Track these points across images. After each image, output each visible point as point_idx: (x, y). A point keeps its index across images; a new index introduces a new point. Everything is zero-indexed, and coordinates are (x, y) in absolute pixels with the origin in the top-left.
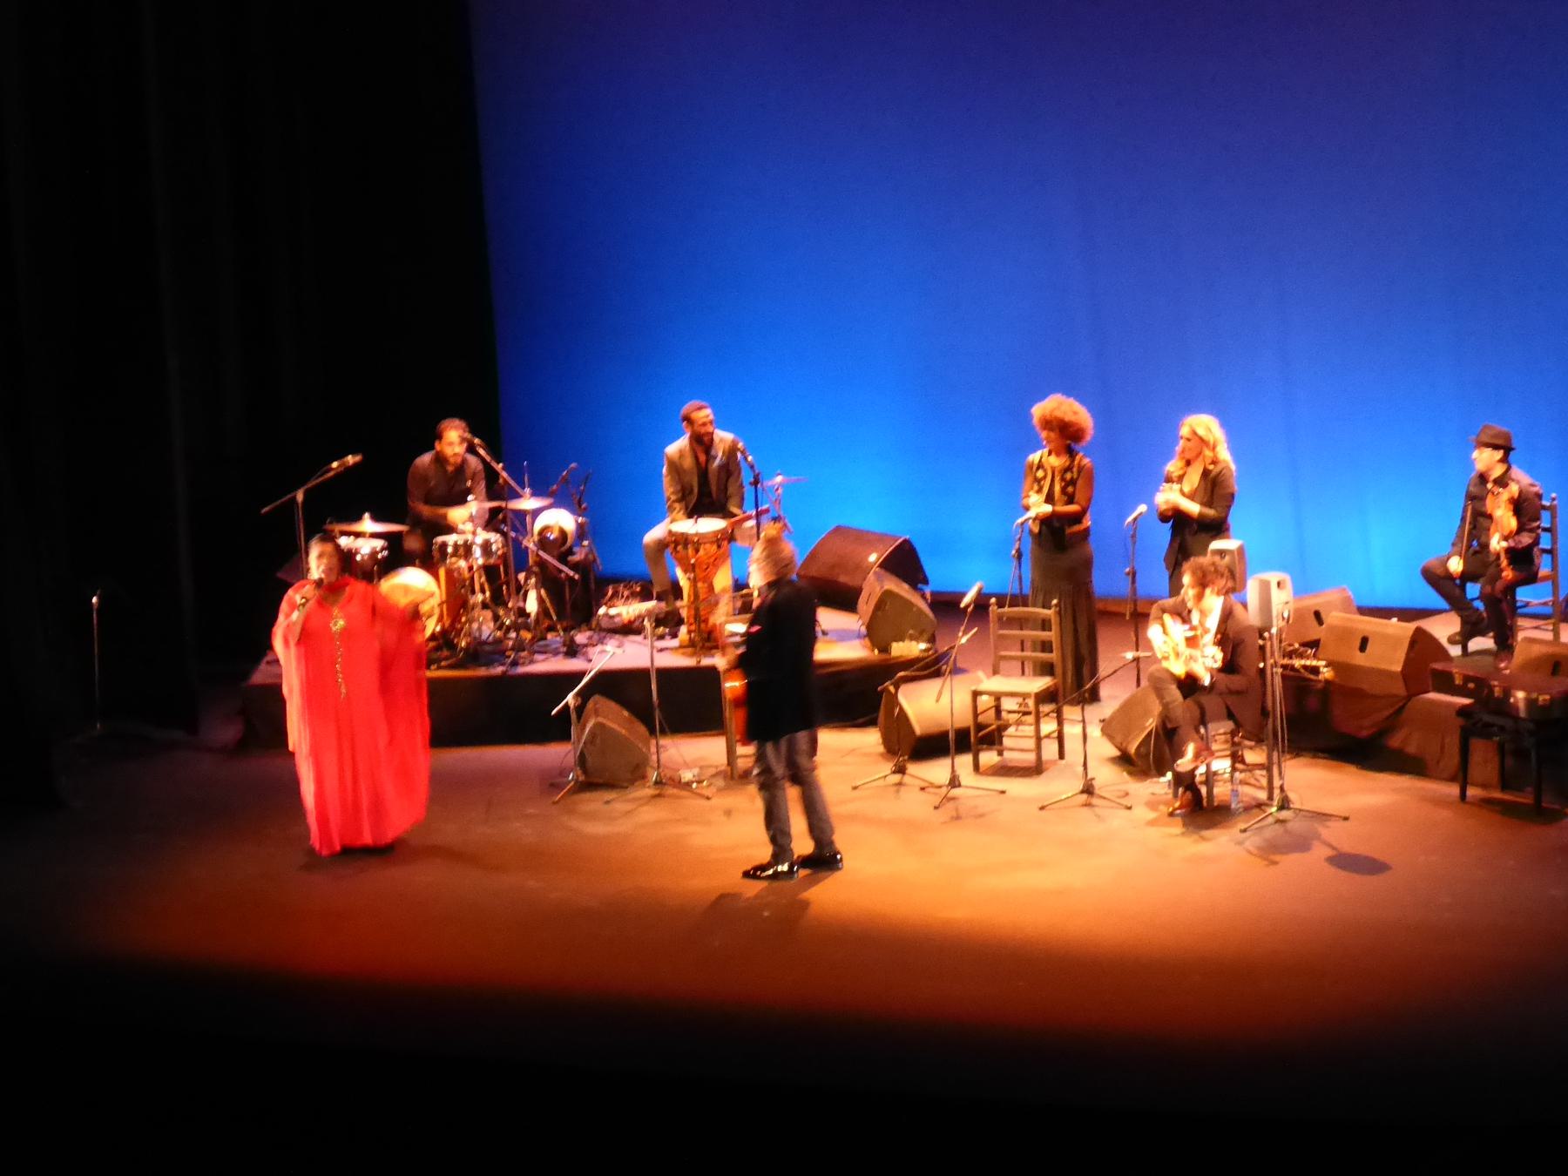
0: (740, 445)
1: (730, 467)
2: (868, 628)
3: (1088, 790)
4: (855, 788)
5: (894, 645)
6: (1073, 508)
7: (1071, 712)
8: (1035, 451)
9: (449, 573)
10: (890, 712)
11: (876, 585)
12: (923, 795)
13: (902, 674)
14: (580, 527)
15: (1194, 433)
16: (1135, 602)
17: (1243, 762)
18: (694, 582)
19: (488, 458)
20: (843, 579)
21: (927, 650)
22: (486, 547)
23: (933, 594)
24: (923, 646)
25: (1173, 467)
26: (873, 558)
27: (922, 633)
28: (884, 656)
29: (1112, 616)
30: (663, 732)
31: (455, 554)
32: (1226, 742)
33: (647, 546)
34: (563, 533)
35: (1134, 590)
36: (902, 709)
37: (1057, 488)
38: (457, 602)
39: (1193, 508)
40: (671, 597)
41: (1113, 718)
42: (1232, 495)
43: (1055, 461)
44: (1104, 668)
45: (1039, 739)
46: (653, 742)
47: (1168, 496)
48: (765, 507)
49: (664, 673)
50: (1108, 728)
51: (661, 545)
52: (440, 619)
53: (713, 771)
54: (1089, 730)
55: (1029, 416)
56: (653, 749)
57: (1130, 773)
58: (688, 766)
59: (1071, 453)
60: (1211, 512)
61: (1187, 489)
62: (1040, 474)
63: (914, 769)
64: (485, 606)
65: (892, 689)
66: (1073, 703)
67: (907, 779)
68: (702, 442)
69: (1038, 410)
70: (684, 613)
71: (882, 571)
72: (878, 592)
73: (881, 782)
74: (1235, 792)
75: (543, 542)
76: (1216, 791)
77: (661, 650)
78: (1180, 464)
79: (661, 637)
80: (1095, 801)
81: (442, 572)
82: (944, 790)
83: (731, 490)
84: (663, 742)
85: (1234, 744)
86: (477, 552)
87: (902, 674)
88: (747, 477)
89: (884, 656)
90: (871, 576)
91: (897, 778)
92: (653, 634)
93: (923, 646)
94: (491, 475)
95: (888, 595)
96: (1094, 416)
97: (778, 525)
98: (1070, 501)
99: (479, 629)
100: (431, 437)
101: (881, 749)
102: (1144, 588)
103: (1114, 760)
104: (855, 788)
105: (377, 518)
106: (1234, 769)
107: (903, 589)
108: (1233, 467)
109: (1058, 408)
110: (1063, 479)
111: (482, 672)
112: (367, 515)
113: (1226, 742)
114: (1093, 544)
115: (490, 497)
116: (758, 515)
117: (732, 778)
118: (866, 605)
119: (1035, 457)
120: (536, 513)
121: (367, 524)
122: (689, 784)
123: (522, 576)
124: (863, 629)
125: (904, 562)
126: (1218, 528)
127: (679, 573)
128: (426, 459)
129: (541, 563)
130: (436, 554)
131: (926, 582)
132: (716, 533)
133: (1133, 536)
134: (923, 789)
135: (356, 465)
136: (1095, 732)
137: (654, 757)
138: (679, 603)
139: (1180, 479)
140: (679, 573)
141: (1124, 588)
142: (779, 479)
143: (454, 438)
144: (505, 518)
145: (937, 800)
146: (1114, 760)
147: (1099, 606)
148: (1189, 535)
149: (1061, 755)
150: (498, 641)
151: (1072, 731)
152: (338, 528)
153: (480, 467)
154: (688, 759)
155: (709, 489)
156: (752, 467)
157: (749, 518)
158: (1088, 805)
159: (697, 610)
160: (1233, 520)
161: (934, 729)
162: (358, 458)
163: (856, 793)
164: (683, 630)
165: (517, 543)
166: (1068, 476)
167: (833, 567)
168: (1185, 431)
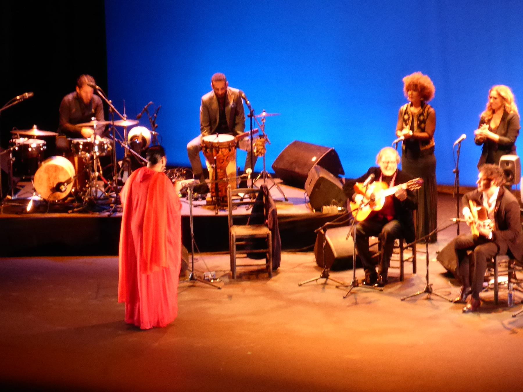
0: (243, 95)
1: (237, 110)
2: (310, 198)
3: (428, 290)
4: (300, 285)
5: (324, 207)
6: (424, 135)
7: (420, 248)
8: (404, 104)
9: (80, 159)
10: (320, 244)
11: (315, 174)
12: (337, 290)
13: (328, 223)
14: (153, 137)
15: (499, 95)
16: (458, 188)
17: (515, 278)
18: (215, 169)
19: (104, 97)
20: (297, 170)
21: (341, 211)
22: (101, 145)
23: (346, 179)
24: (340, 208)
25: (485, 114)
26: (314, 159)
27: (340, 201)
28: (319, 213)
29: (445, 195)
30: (196, 252)
31: (84, 149)
32: (506, 267)
33: (189, 150)
34: (144, 139)
35: (457, 181)
36: (327, 243)
37: (415, 125)
38: (83, 175)
39: (496, 137)
40: (203, 176)
41: (443, 251)
42: (518, 132)
43: (414, 110)
44: (441, 224)
45: (402, 261)
46: (190, 256)
47: (484, 131)
48: (256, 129)
49: (197, 219)
50: (440, 257)
51: (197, 149)
52: (74, 185)
53: (222, 273)
54: (430, 257)
55: (402, 84)
56: (190, 261)
57: (452, 282)
58: (209, 270)
59: (422, 105)
60: (506, 139)
61: (493, 125)
62: (406, 117)
63: (332, 275)
64: (99, 178)
65: (322, 231)
66: (422, 242)
67: (329, 281)
68: (222, 99)
69: (407, 80)
70: (210, 186)
71: (319, 167)
72: (316, 178)
73: (315, 283)
74: (510, 295)
75: (133, 145)
76: (500, 293)
77: (196, 206)
78: (489, 113)
79: (196, 199)
80: (432, 297)
81: (76, 159)
82: (349, 288)
83: (237, 121)
84: (196, 256)
85: (509, 267)
86: (96, 149)
87: (328, 223)
88: (247, 112)
89: (319, 213)
90: (313, 169)
91: (323, 280)
92: (192, 197)
93: (340, 208)
94: (106, 106)
95: (322, 179)
96: (436, 88)
97: (262, 140)
98: (423, 130)
99: (96, 191)
100: (74, 84)
101: (315, 264)
102: (464, 180)
103: (445, 275)
104: (300, 285)
105: (40, 128)
106: (510, 281)
107: (330, 177)
108: (519, 116)
109: (418, 80)
110: (418, 120)
111: (97, 215)
112: (35, 126)
113: (506, 267)
114: (437, 155)
115: (106, 119)
116: (252, 133)
117: (233, 278)
118: (309, 185)
119: (404, 108)
120: (129, 128)
121: (35, 132)
122: (209, 280)
123: (120, 163)
124: (308, 198)
125: (331, 162)
126: (509, 148)
127: (208, 164)
128: (70, 97)
129: (132, 156)
130: (73, 149)
131: (343, 173)
132: (228, 143)
133: (458, 152)
134: (337, 287)
135: (30, 98)
136: (433, 259)
137: (191, 265)
138: (207, 181)
139: (489, 121)
140: (208, 164)
141: (452, 180)
142: (264, 114)
143: (87, 88)
144: (112, 129)
145: (345, 293)
146: (445, 275)
147: (439, 189)
148: (491, 150)
149: (414, 271)
150: (106, 198)
151: (421, 258)
152: (19, 132)
153: (101, 102)
154: (209, 266)
155: (225, 117)
156: (249, 107)
157: (247, 135)
158: (428, 299)
159: (217, 184)
160: (518, 144)
161: (345, 254)
162: (31, 94)
163: (300, 287)
164: (209, 195)
165: (118, 144)
166: (422, 118)
167: (292, 163)
168: (494, 93)
